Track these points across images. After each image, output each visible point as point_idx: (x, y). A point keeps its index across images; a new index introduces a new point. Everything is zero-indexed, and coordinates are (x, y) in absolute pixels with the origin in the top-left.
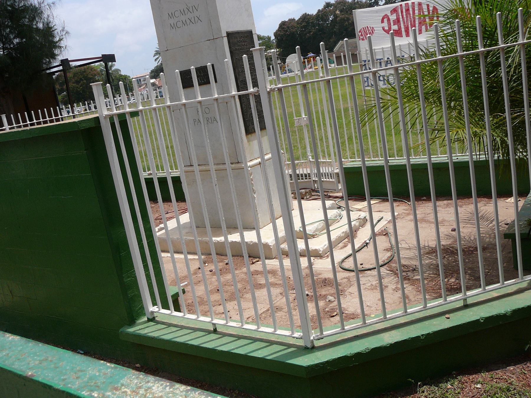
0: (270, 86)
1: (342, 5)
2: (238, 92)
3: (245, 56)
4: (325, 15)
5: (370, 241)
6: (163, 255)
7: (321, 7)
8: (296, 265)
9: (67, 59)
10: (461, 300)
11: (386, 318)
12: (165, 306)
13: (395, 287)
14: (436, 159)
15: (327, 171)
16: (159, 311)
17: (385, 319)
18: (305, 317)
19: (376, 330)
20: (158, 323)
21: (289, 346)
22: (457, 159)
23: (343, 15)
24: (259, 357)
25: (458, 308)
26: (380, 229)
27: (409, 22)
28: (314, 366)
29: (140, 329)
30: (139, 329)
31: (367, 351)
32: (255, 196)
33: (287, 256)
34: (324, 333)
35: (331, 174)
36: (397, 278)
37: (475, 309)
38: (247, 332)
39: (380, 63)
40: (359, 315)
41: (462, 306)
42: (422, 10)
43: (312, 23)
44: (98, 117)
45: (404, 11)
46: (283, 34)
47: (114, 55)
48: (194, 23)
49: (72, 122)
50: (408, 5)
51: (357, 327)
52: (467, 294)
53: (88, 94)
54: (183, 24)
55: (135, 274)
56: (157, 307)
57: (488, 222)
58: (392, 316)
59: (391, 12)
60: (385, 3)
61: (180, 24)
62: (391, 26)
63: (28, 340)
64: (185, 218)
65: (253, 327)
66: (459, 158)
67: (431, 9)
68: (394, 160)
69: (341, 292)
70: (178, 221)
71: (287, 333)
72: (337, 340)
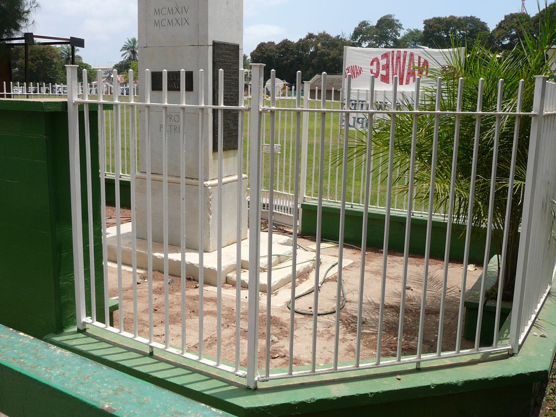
0: (263, 106)
1: (325, 39)
2: (213, 105)
3: (221, 70)
4: (306, 46)
5: (321, 285)
6: (109, 264)
7: (303, 37)
8: (254, 300)
9: (32, 33)
10: (414, 362)
11: (337, 369)
12: (101, 318)
13: (342, 337)
14: (396, 212)
15: (287, 205)
16: (93, 322)
17: (335, 370)
18: (253, 356)
19: (324, 381)
20: (89, 335)
21: (230, 383)
22: (422, 216)
23: (324, 48)
24: (197, 390)
25: (410, 370)
26: (334, 274)
27: (398, 70)
28: (254, 409)
29: (67, 340)
30: (66, 339)
31: (312, 401)
32: (211, 218)
33: (233, 286)
34: (270, 375)
35: (290, 209)
36: (346, 329)
37: (427, 374)
38: (186, 361)
39: (362, 105)
40: (302, 361)
41: (414, 369)
42: (413, 61)
43: (291, 50)
44: (66, 102)
45: (395, 58)
46: (260, 55)
47: (84, 40)
48: (181, 25)
49: (36, 102)
50: (400, 53)
51: (305, 374)
52: (421, 357)
53: (42, 76)
54: (169, 24)
55: (74, 278)
56: (91, 319)
57: (438, 286)
58: (343, 369)
59: (382, 56)
60: (368, 46)
61: (165, 22)
62: (379, 71)
63: (85, 359)
64: (127, 228)
65: (195, 357)
66: (423, 215)
67: (422, 61)
68: (402, 211)
69: (286, 333)
70: (118, 230)
71: (231, 369)
72: (282, 385)
